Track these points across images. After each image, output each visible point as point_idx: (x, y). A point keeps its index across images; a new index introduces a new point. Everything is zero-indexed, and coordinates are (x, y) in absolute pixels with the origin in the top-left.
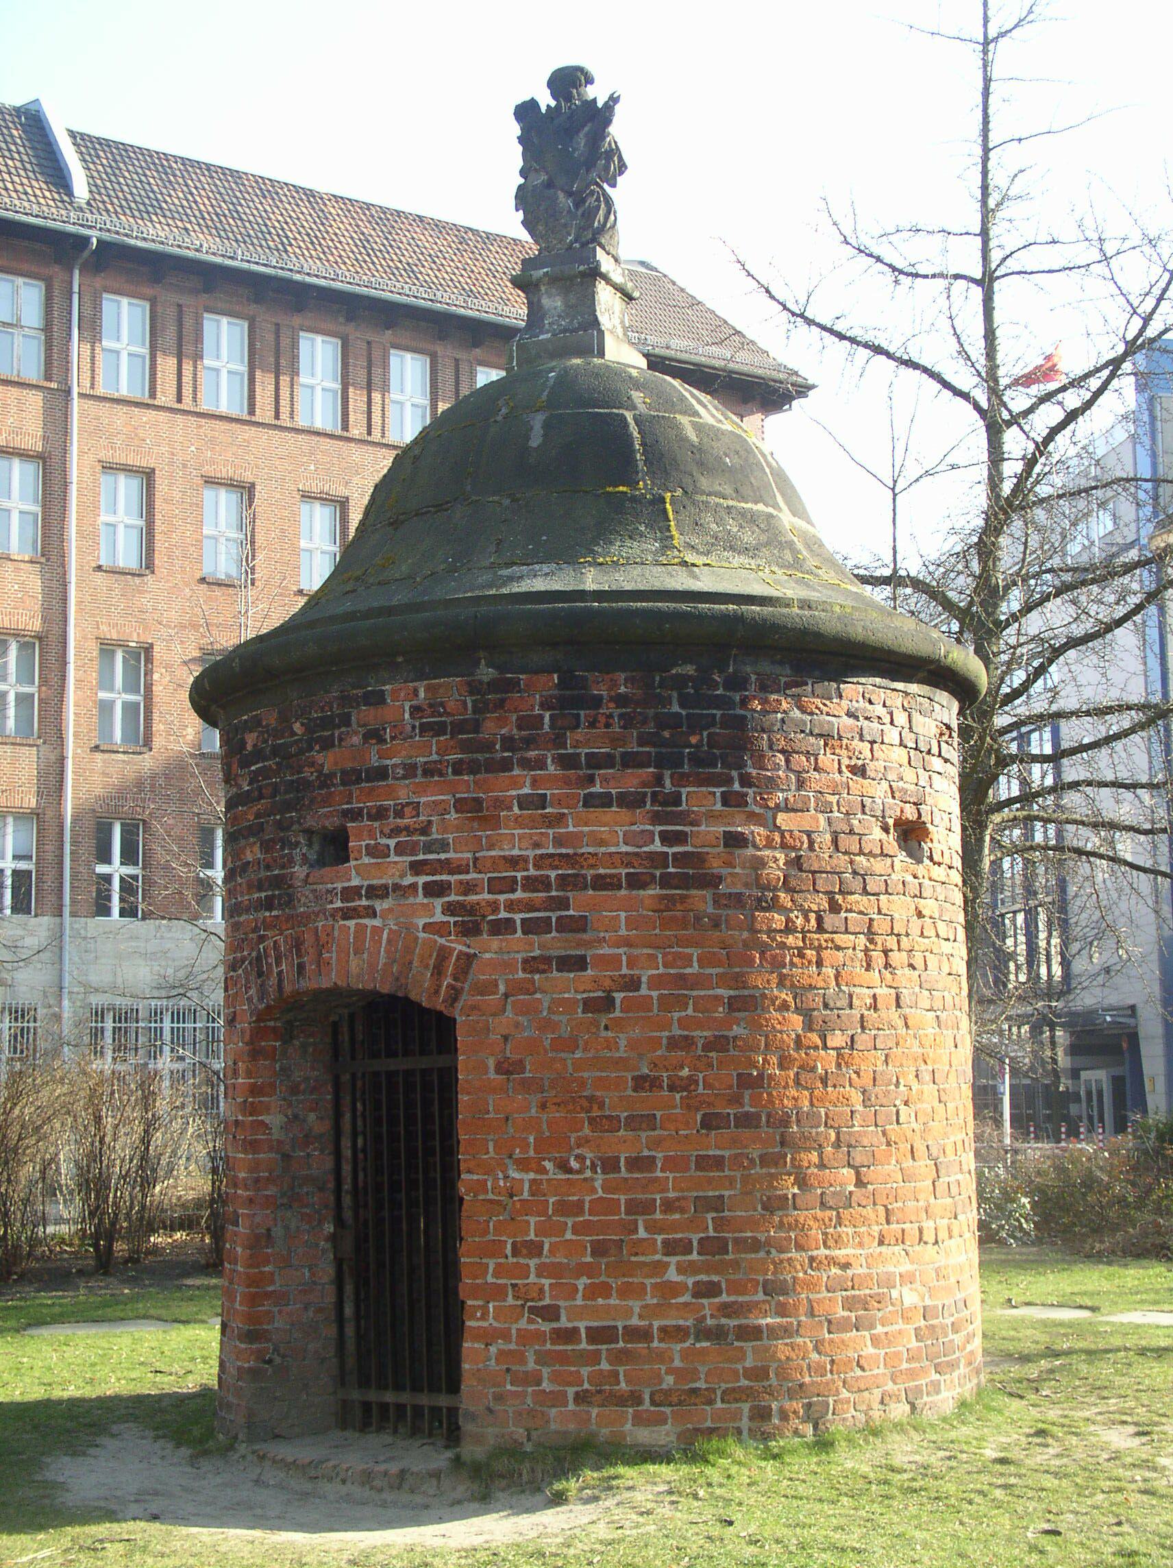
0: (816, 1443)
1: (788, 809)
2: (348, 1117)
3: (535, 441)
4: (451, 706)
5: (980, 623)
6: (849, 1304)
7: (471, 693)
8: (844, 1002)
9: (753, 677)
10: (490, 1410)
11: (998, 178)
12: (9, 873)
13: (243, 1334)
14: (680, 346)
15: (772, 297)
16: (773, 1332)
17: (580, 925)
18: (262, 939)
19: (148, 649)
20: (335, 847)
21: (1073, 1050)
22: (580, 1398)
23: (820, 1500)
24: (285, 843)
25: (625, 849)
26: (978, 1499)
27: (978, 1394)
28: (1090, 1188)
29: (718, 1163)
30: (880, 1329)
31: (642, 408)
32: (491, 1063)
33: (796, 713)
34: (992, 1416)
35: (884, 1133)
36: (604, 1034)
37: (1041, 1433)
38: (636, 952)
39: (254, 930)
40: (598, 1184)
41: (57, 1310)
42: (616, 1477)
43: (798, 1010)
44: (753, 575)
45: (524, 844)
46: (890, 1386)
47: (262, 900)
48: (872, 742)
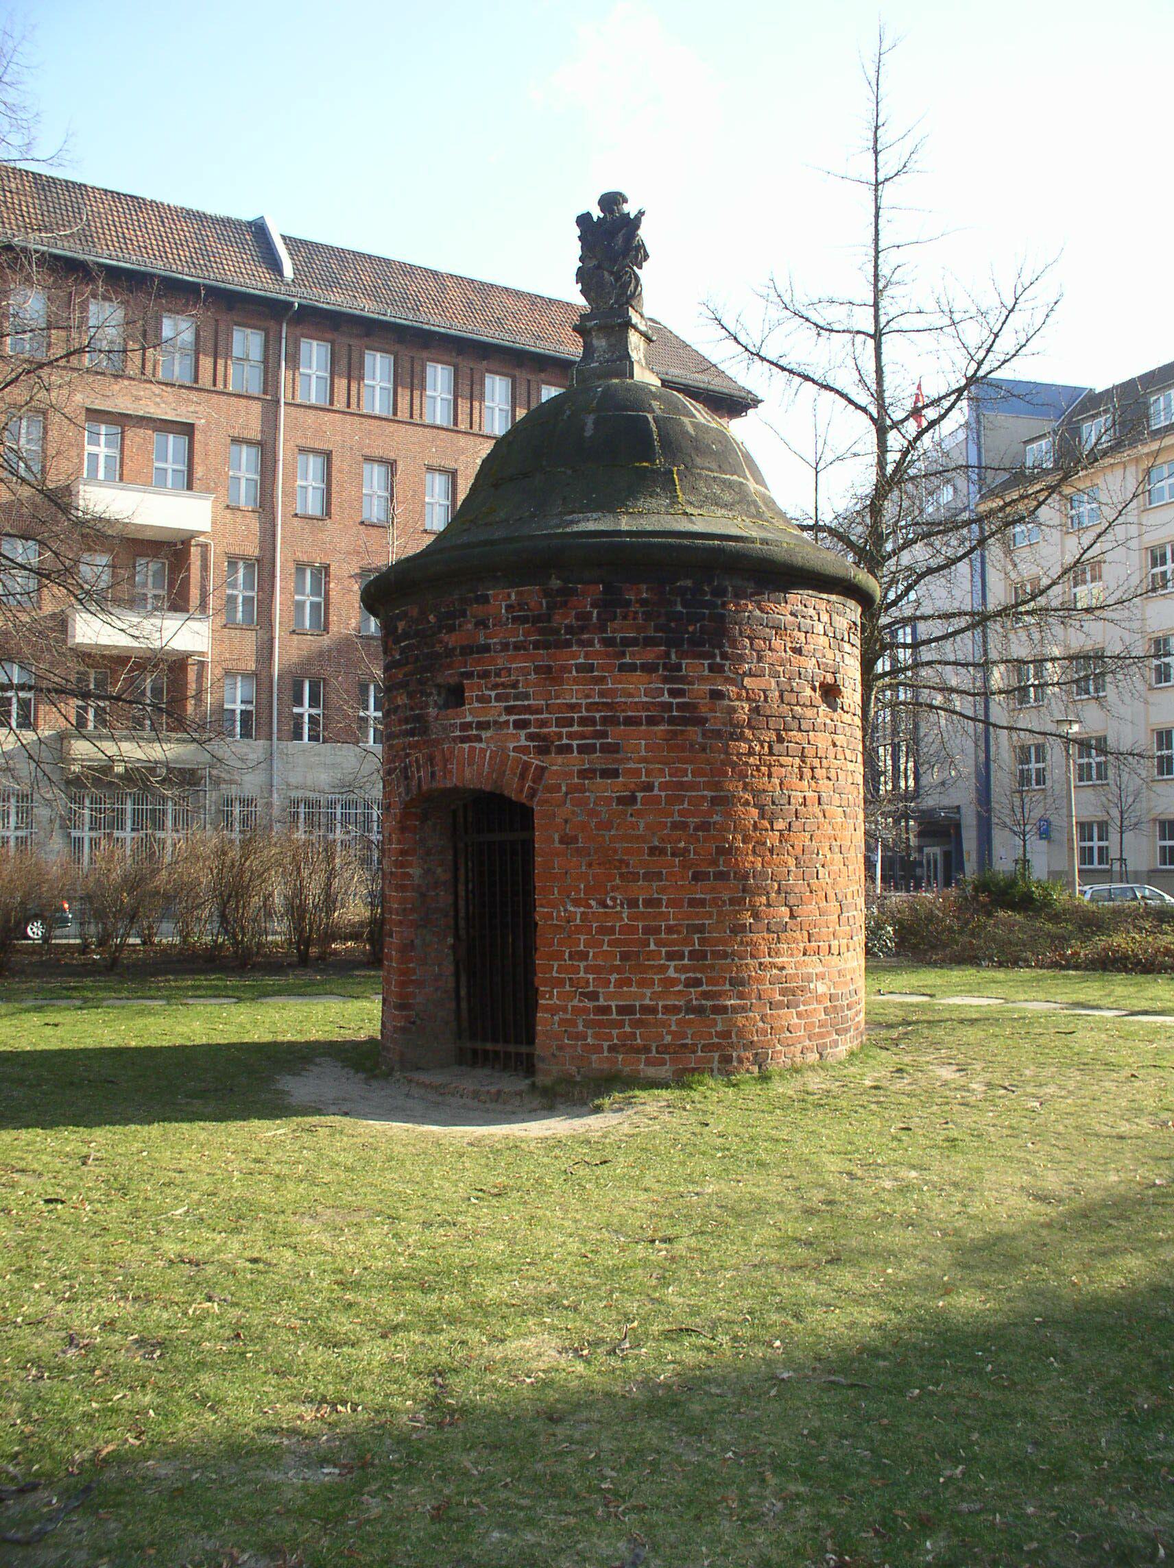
0: (760, 1077)
1: (751, 675)
2: (462, 871)
3: (589, 432)
4: (532, 605)
5: (872, 559)
6: (783, 992)
7: (545, 597)
8: (785, 801)
9: (730, 589)
10: (553, 1055)
11: (884, 270)
12: (238, 712)
13: (396, 1006)
14: (677, 373)
15: (739, 343)
16: (735, 1009)
17: (613, 749)
18: (408, 755)
19: (327, 568)
20: (456, 696)
21: (920, 835)
22: (612, 1049)
23: (763, 1111)
24: (423, 693)
25: (645, 699)
26: (860, 1110)
27: (862, 1048)
28: (930, 921)
29: (702, 903)
30: (802, 1008)
31: (658, 412)
32: (556, 837)
33: (758, 613)
34: (869, 1060)
35: (809, 885)
36: (630, 819)
37: (900, 1070)
38: (652, 766)
39: (404, 749)
40: (624, 915)
41: (276, 988)
42: (634, 1097)
43: (755, 806)
44: (730, 522)
45: (580, 696)
46: (807, 1043)
47: (407, 731)
48: (806, 632)
